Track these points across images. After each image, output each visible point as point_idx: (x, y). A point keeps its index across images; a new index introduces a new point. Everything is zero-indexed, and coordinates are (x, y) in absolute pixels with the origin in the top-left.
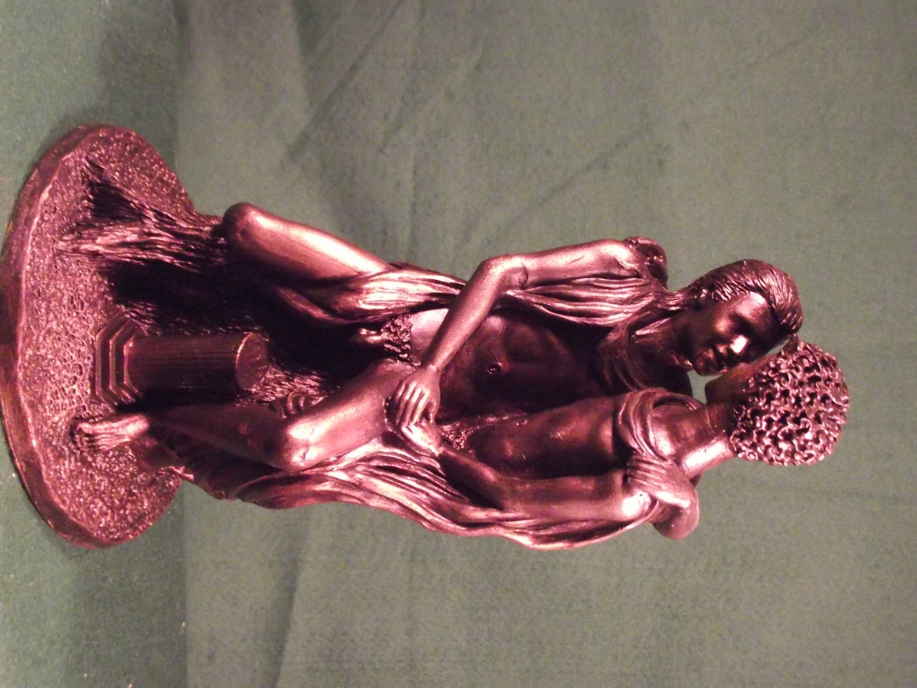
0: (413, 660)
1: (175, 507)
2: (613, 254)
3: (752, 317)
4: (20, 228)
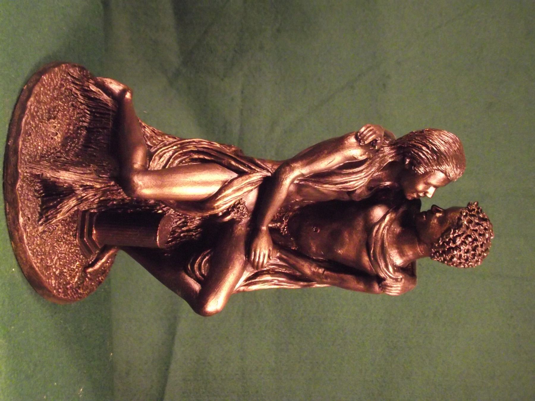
0: (244, 374)
1: (106, 287)
4: (19, 245)
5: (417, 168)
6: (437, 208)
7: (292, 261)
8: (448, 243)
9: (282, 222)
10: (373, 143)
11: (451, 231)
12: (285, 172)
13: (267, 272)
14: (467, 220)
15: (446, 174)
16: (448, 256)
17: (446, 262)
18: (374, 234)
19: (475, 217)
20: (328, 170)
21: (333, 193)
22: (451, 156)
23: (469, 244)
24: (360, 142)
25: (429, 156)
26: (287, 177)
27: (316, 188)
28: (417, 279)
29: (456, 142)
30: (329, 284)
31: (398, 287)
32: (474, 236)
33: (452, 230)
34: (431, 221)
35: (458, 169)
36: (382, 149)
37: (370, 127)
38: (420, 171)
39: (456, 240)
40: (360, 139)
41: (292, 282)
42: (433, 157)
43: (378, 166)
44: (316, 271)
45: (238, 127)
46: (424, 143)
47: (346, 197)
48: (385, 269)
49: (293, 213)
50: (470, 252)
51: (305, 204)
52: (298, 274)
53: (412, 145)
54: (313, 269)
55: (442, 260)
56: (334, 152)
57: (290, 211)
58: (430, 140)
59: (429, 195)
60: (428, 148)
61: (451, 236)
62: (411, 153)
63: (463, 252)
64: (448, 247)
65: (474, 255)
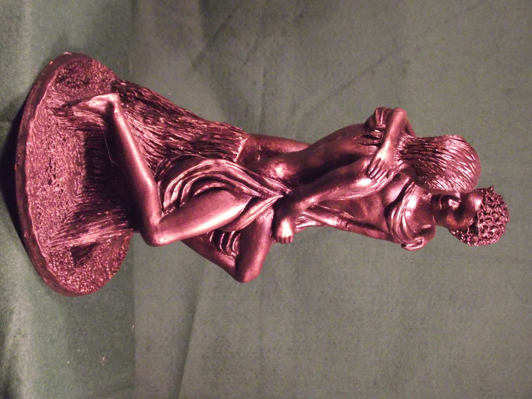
45: (260, 110)
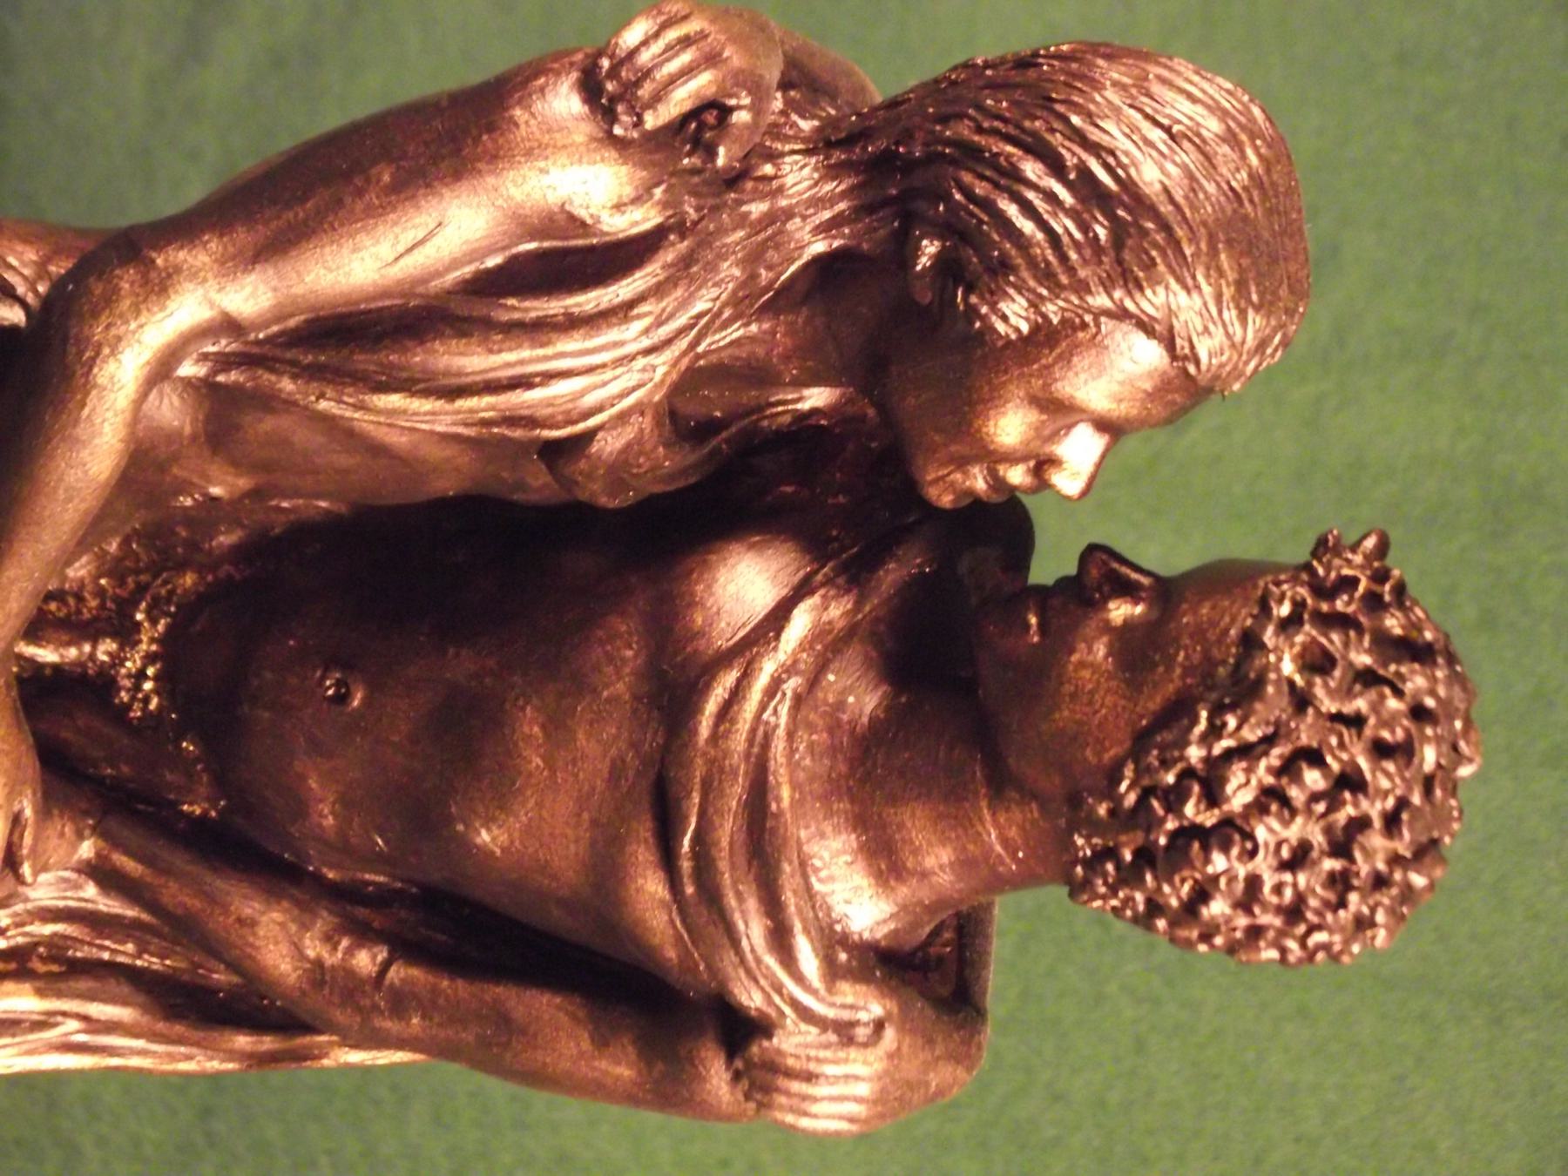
2: (554, 199)
3: (1114, 406)
5: (982, 297)
6: (1115, 565)
7: (175, 895)
8: (1174, 799)
9: (126, 634)
10: (702, 126)
11: (1195, 721)
12: (110, 299)
13: (13, 966)
14: (1297, 649)
15: (1169, 342)
16: (1171, 884)
17: (1161, 924)
18: (705, 728)
19: (1352, 634)
20: (403, 295)
21: (448, 451)
22: (1204, 223)
23: (1309, 811)
24: (610, 116)
25: (1064, 225)
26: (119, 339)
27: (328, 420)
28: (989, 1031)
29: (1244, 137)
30: (414, 1049)
31: (856, 1078)
32: (1345, 756)
33: (1204, 714)
34: (1072, 651)
35: (1251, 314)
36: (768, 169)
37: (685, 18)
38: (1005, 318)
39: (1223, 781)
40: (613, 99)
41: (179, 1029)
42: (1085, 228)
43: (733, 278)
44: (332, 959)
46: (1034, 134)
47: (538, 483)
48: (770, 961)
49: (202, 578)
50: (1315, 863)
51: (283, 518)
52: (220, 977)
53: (956, 143)
54: (314, 948)
55: (1141, 908)
56: (441, 179)
57: (181, 567)
58: (1076, 120)
59: (1069, 481)
60: (1056, 167)
61: (1195, 753)
62: (948, 198)
63: (1272, 861)
64: (1171, 825)
65: (1340, 883)
